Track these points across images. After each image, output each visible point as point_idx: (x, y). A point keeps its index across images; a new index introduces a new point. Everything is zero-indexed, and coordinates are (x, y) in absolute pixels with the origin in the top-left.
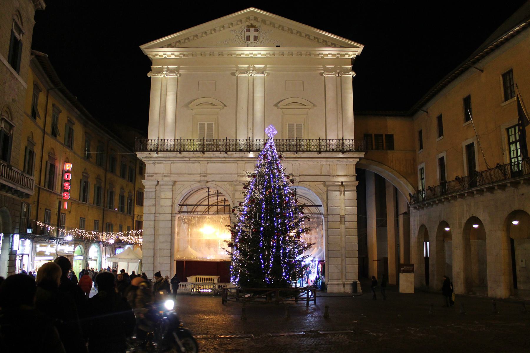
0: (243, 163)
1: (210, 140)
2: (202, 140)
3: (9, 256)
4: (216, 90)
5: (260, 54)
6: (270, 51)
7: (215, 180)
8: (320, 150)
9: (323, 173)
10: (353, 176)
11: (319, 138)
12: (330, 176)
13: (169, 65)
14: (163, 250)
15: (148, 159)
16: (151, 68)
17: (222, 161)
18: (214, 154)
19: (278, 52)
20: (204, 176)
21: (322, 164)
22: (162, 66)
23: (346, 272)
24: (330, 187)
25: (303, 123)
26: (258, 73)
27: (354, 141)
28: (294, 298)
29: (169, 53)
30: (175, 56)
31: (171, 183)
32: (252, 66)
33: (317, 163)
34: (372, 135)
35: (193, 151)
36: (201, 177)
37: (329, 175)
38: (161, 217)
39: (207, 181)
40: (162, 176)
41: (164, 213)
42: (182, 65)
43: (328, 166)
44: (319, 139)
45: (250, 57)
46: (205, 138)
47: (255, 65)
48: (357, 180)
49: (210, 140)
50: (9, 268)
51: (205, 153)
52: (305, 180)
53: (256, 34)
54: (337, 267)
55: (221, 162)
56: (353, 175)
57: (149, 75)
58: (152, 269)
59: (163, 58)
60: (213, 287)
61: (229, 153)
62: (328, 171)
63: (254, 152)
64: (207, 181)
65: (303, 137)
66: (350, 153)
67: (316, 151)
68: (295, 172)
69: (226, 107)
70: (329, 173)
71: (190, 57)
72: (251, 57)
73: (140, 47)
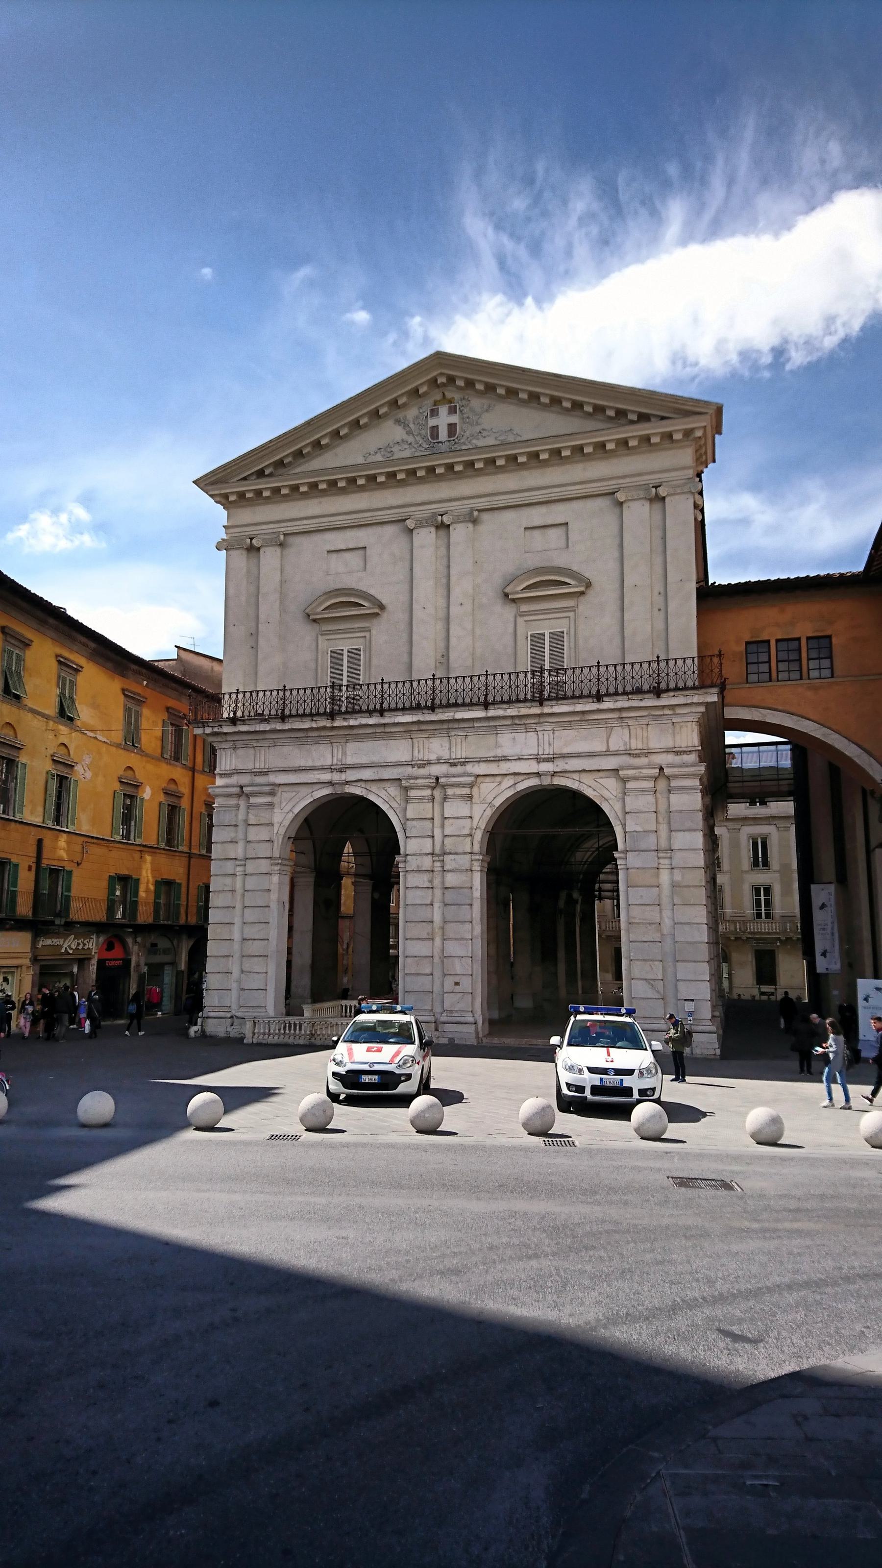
1: (557, 673)
2: (537, 674)
4: (365, 569)
8: (598, 691)
9: (612, 748)
10: (690, 751)
11: (598, 663)
12: (630, 754)
14: (250, 942)
15: (219, 739)
21: (609, 725)
24: (630, 783)
25: (362, 647)
27: (696, 659)
33: (597, 726)
34: (768, 642)
35: (311, 715)
36: (334, 773)
37: (628, 752)
38: (440, 869)
40: (251, 775)
43: (626, 731)
44: (599, 665)
46: (547, 667)
48: (701, 761)
49: (557, 673)
51: (386, 714)
52: (568, 768)
53: (454, 419)
54: (652, 986)
56: (690, 749)
62: (625, 744)
65: (361, 680)
66: (676, 694)
67: (590, 696)
68: (544, 750)
70: (628, 746)
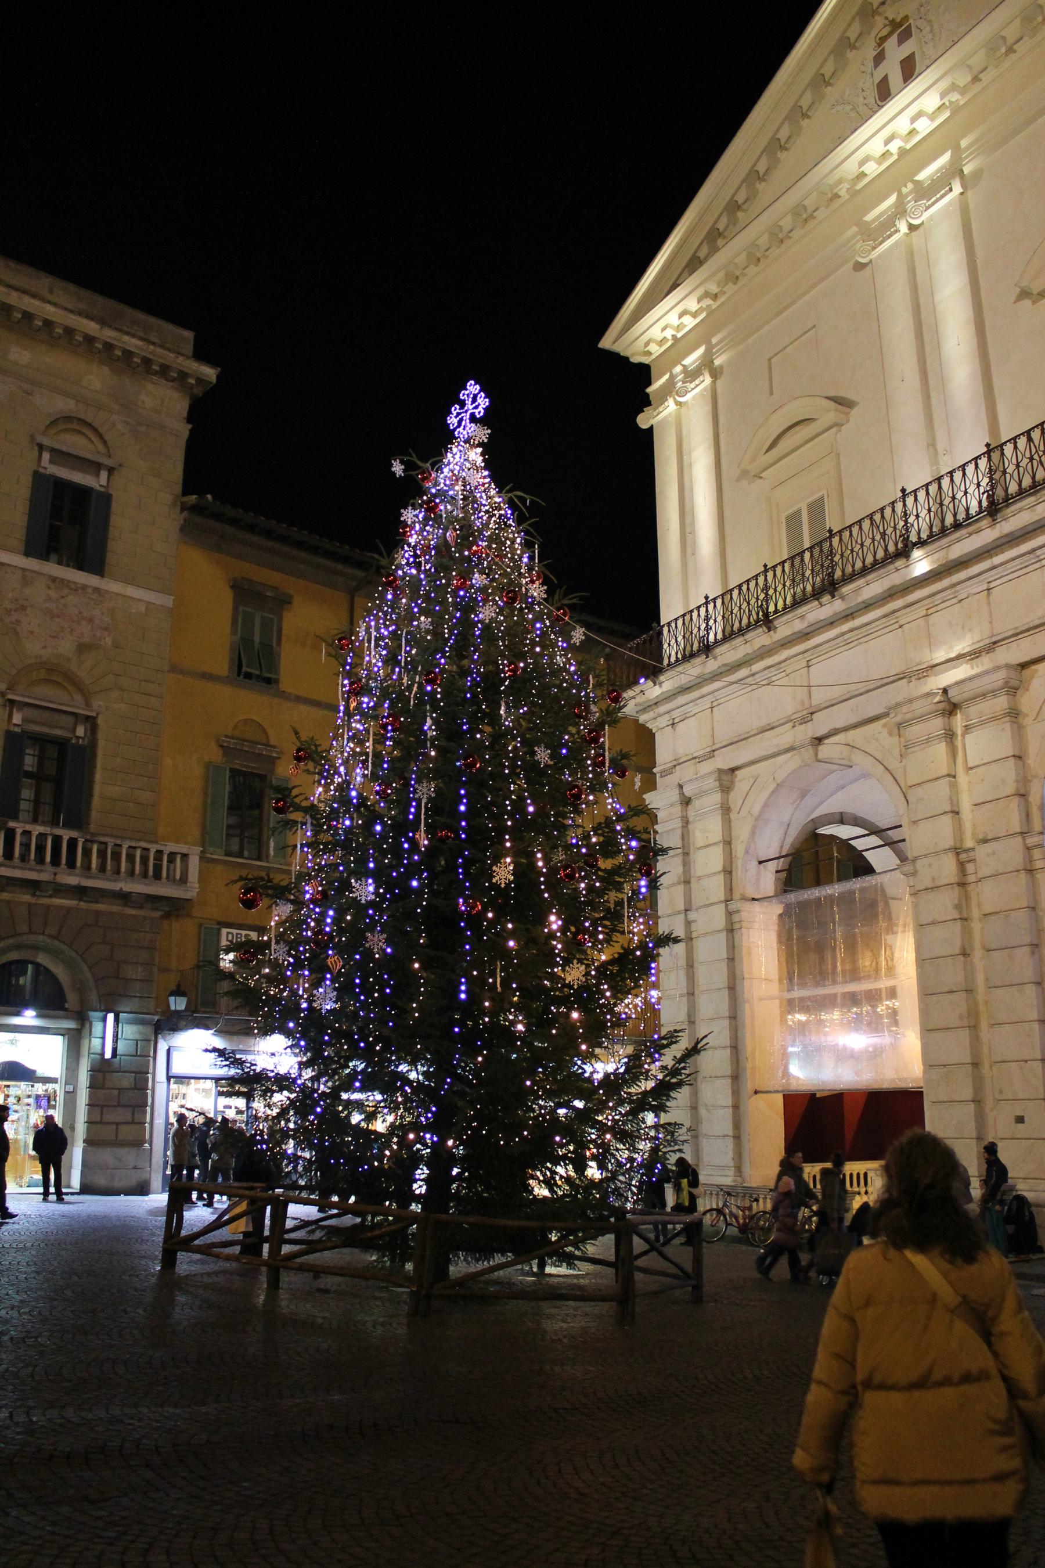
0: (918, 616)
3: (91, 1075)
5: (920, 114)
6: (945, 74)
7: (839, 725)
13: (683, 359)
16: (648, 395)
17: (846, 636)
18: (802, 617)
19: (982, 54)
20: (804, 721)
22: (671, 373)
23: (102, 1108)
26: (934, 199)
28: (550, 1275)
29: (673, 318)
30: (694, 315)
31: (711, 782)
32: (910, 186)
39: (819, 740)
41: (707, 903)
42: (714, 334)
45: (895, 157)
47: (916, 174)
50: (89, 1110)
55: (845, 642)
57: (643, 421)
58: (971, 1129)
59: (670, 343)
60: (725, 1205)
61: (845, 590)
63: (928, 548)
64: (819, 740)
69: (856, 409)
71: (730, 289)
72: (903, 153)
73: (600, 345)
